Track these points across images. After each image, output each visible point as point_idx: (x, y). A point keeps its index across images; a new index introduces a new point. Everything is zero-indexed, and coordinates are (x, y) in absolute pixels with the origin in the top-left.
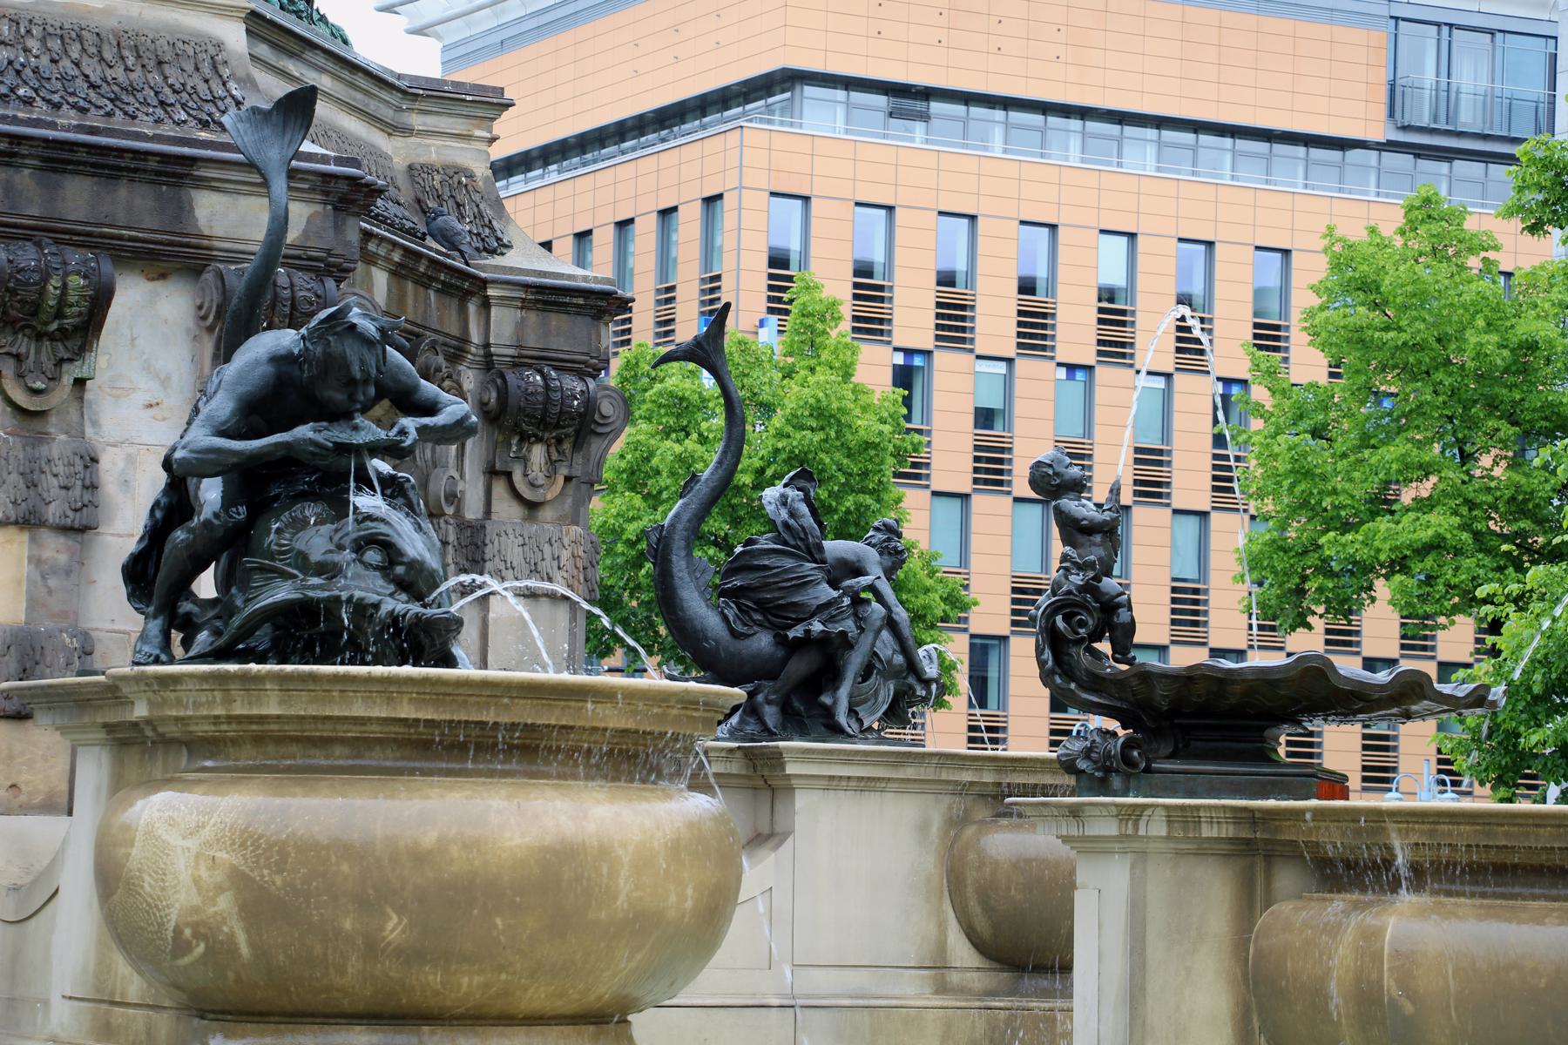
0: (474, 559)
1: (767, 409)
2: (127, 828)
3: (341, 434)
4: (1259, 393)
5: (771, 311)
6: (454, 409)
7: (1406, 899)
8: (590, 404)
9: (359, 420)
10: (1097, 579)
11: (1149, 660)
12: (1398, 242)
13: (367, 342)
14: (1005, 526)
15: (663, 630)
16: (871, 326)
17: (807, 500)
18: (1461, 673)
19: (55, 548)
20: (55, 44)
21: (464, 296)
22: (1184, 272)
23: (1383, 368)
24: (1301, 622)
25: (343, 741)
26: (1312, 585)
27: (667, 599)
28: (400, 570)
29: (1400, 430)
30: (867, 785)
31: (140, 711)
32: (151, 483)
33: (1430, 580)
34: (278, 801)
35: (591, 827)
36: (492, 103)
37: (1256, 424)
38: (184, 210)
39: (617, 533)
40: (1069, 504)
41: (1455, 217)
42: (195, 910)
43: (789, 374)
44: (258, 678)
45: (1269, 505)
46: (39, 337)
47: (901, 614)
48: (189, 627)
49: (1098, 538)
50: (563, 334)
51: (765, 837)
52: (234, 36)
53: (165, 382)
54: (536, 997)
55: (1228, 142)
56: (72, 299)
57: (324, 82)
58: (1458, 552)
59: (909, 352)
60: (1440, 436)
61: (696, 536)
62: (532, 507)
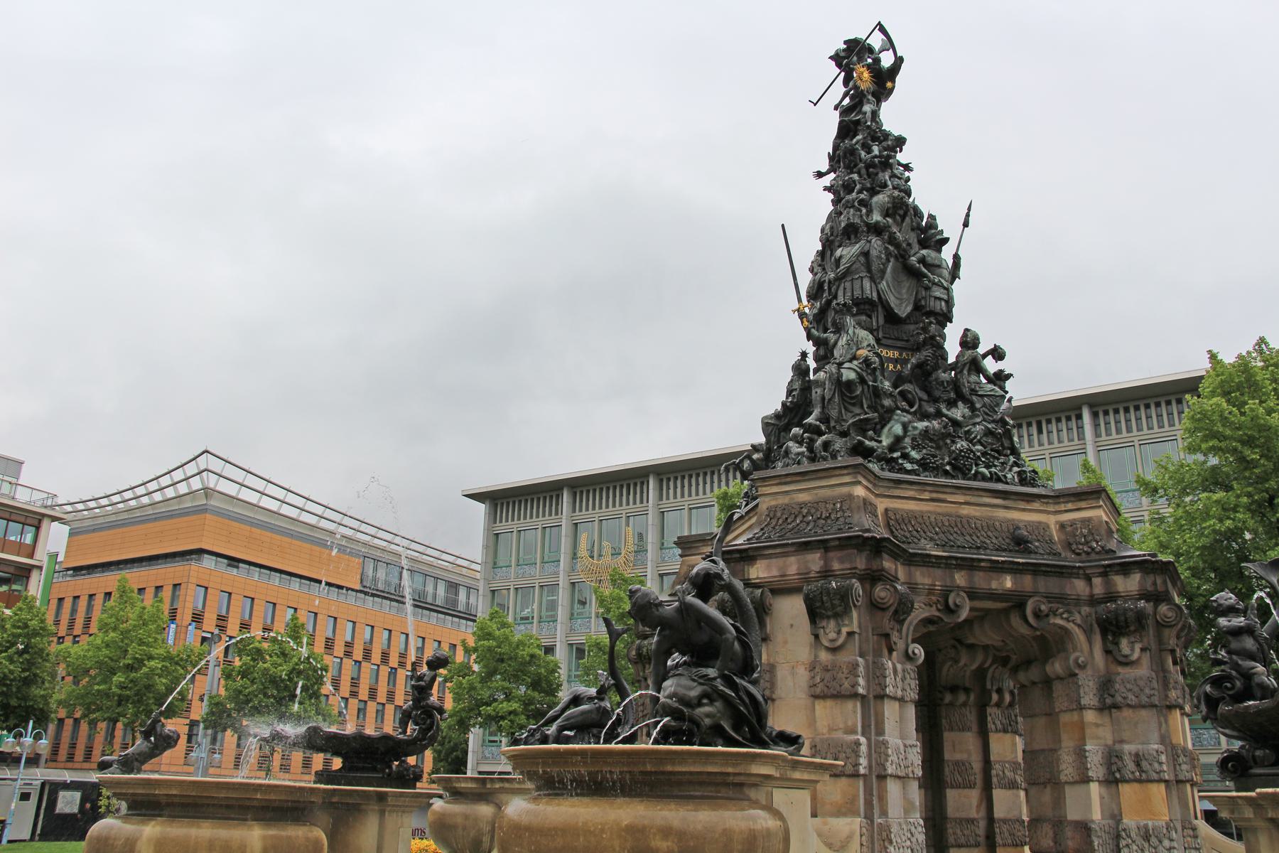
5: (193, 621)
39: (240, 692)
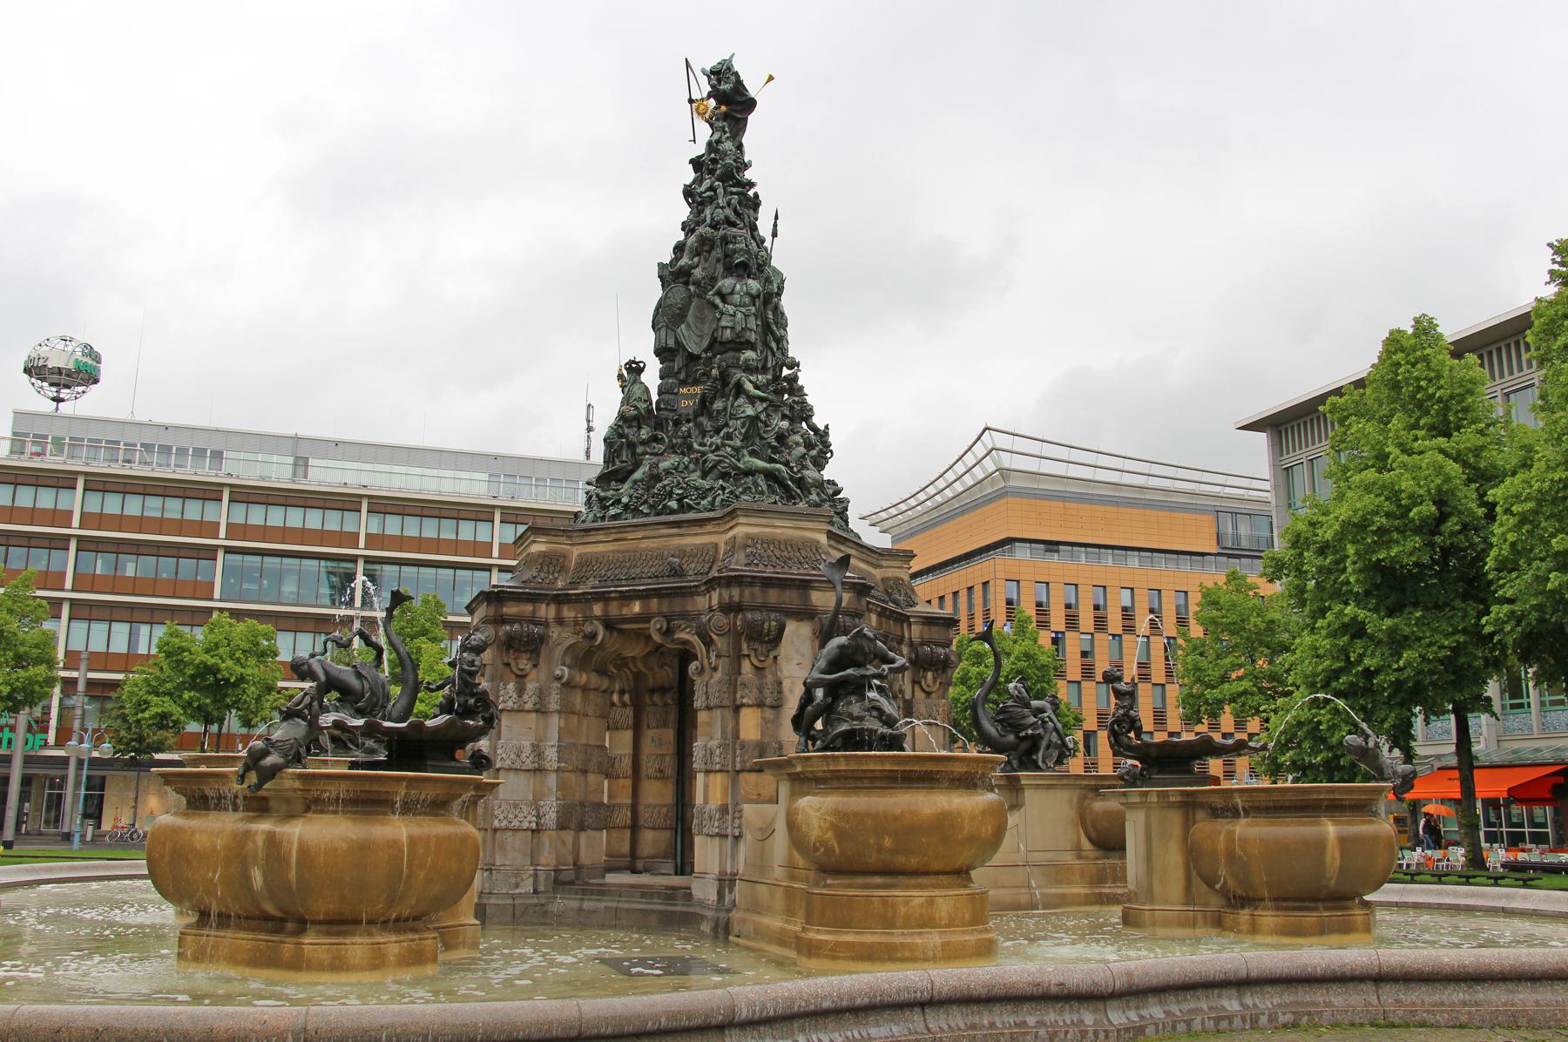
0: (908, 710)
1: (1008, 655)
2: (796, 809)
3: (863, 672)
4: (1180, 641)
6: (901, 661)
7: (1243, 821)
8: (947, 657)
9: (868, 667)
10: (1128, 711)
11: (1146, 738)
12: (1225, 587)
13: (869, 639)
14: (1094, 692)
15: (975, 733)
16: (1043, 624)
17: (1024, 687)
18: (1256, 738)
19: (769, 713)
20: (765, 545)
21: (902, 622)
22: (1151, 601)
23: (1222, 631)
24: (1199, 721)
25: (868, 778)
26: (1203, 709)
27: (976, 723)
28: (884, 718)
29: (1230, 652)
30: (1050, 787)
31: (799, 769)
32: (800, 690)
33: (1244, 705)
34: (846, 799)
35: (954, 806)
36: (909, 555)
37: (1180, 652)
38: (808, 597)
39: (957, 700)
40: (1117, 685)
41: (1244, 578)
42: (819, 837)
43: (1015, 642)
44: (838, 757)
45: (1186, 681)
46: (762, 642)
47: (1059, 726)
48: (814, 739)
49: (1127, 697)
50: (936, 633)
51: (1015, 806)
52: (823, 539)
53: (803, 656)
54: (937, 865)
55: (1163, 555)
56: (772, 629)
57: (852, 552)
58: (1253, 694)
59: (1056, 633)
60: (1244, 654)
61: (986, 700)
62: (928, 694)
